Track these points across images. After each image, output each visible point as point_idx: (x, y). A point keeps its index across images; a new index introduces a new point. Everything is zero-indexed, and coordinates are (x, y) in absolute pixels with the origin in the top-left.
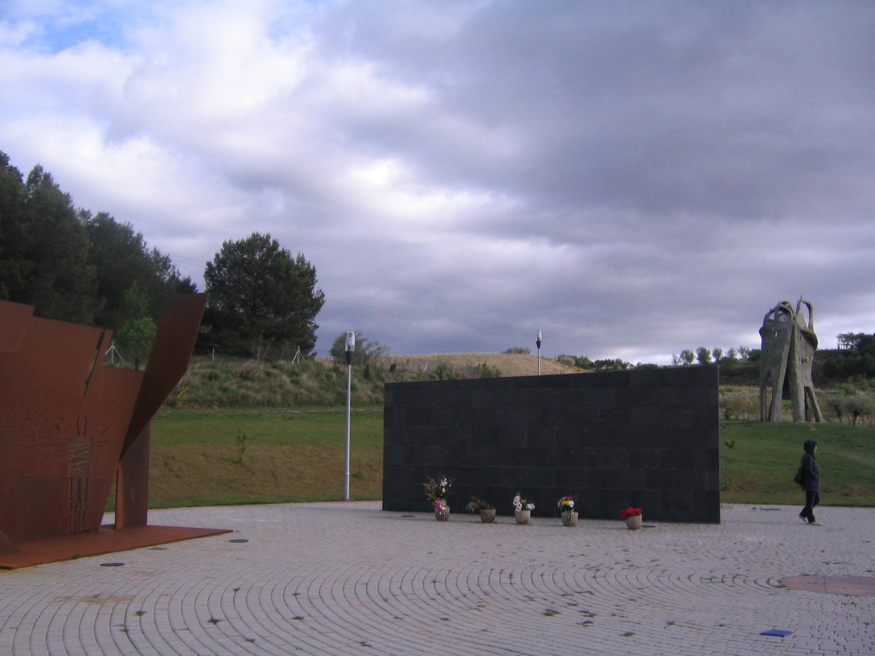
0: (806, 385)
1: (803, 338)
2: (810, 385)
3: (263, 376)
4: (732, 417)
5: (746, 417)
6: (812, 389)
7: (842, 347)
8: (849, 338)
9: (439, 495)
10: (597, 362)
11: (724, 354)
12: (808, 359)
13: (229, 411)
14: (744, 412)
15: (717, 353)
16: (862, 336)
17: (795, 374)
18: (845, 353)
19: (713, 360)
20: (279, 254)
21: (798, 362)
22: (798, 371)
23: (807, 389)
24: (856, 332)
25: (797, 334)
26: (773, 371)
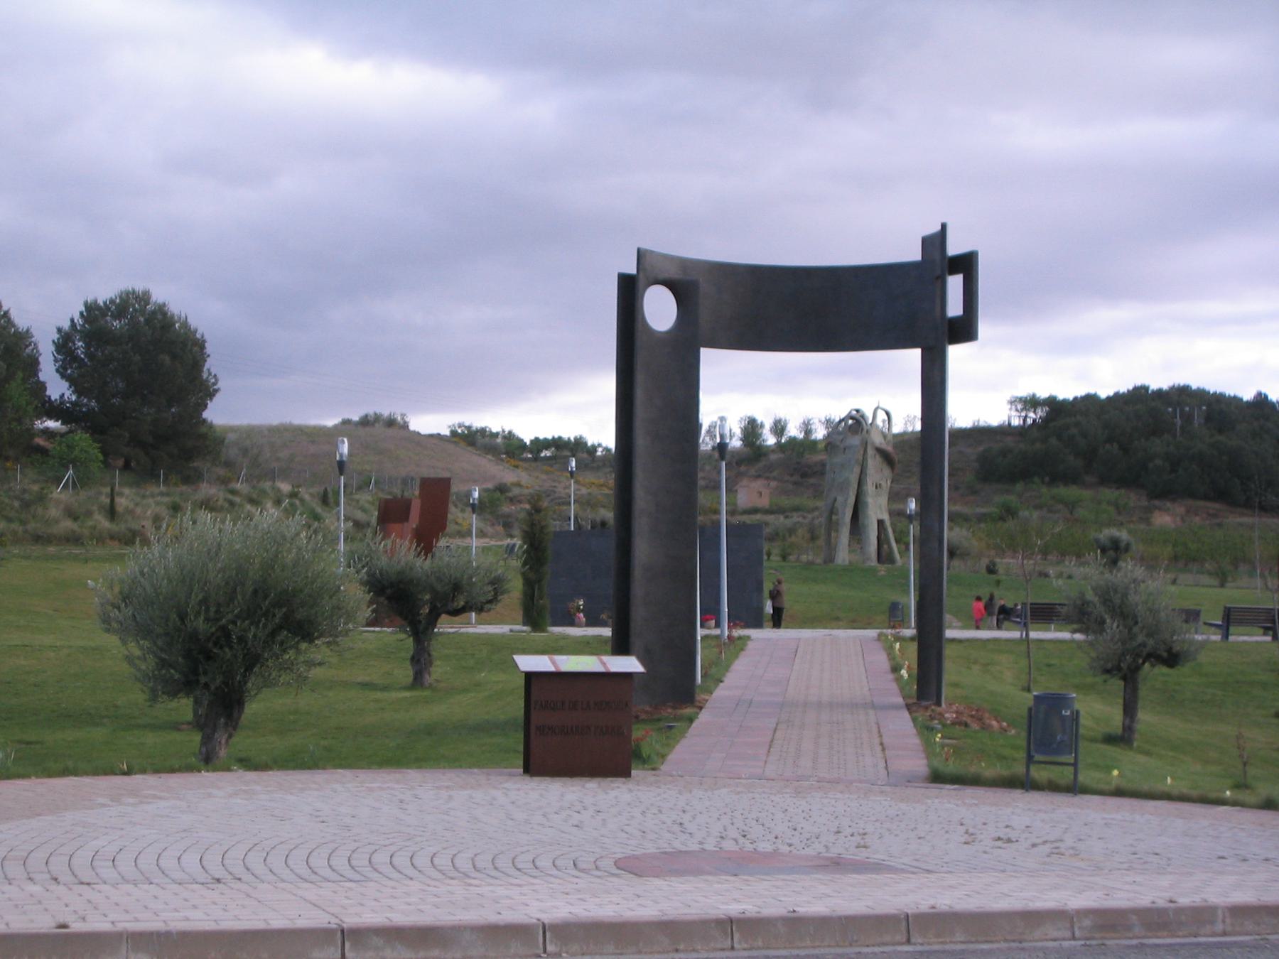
0: (880, 517)
1: (878, 456)
2: (886, 517)
3: (226, 505)
4: (792, 558)
5: (810, 558)
6: (888, 524)
7: (1016, 422)
8: (1031, 402)
9: (579, 610)
10: (536, 441)
11: (794, 431)
12: (883, 484)
13: (37, 550)
14: (1063, 554)
15: (779, 428)
16: (1052, 403)
17: (866, 504)
18: (1022, 432)
19: (771, 440)
20: (154, 313)
21: (869, 487)
22: (870, 500)
23: (880, 523)
24: (1043, 394)
25: (870, 452)
26: (840, 499)
